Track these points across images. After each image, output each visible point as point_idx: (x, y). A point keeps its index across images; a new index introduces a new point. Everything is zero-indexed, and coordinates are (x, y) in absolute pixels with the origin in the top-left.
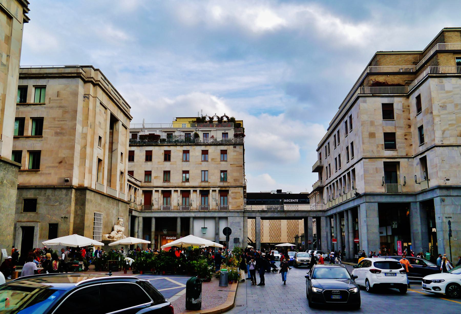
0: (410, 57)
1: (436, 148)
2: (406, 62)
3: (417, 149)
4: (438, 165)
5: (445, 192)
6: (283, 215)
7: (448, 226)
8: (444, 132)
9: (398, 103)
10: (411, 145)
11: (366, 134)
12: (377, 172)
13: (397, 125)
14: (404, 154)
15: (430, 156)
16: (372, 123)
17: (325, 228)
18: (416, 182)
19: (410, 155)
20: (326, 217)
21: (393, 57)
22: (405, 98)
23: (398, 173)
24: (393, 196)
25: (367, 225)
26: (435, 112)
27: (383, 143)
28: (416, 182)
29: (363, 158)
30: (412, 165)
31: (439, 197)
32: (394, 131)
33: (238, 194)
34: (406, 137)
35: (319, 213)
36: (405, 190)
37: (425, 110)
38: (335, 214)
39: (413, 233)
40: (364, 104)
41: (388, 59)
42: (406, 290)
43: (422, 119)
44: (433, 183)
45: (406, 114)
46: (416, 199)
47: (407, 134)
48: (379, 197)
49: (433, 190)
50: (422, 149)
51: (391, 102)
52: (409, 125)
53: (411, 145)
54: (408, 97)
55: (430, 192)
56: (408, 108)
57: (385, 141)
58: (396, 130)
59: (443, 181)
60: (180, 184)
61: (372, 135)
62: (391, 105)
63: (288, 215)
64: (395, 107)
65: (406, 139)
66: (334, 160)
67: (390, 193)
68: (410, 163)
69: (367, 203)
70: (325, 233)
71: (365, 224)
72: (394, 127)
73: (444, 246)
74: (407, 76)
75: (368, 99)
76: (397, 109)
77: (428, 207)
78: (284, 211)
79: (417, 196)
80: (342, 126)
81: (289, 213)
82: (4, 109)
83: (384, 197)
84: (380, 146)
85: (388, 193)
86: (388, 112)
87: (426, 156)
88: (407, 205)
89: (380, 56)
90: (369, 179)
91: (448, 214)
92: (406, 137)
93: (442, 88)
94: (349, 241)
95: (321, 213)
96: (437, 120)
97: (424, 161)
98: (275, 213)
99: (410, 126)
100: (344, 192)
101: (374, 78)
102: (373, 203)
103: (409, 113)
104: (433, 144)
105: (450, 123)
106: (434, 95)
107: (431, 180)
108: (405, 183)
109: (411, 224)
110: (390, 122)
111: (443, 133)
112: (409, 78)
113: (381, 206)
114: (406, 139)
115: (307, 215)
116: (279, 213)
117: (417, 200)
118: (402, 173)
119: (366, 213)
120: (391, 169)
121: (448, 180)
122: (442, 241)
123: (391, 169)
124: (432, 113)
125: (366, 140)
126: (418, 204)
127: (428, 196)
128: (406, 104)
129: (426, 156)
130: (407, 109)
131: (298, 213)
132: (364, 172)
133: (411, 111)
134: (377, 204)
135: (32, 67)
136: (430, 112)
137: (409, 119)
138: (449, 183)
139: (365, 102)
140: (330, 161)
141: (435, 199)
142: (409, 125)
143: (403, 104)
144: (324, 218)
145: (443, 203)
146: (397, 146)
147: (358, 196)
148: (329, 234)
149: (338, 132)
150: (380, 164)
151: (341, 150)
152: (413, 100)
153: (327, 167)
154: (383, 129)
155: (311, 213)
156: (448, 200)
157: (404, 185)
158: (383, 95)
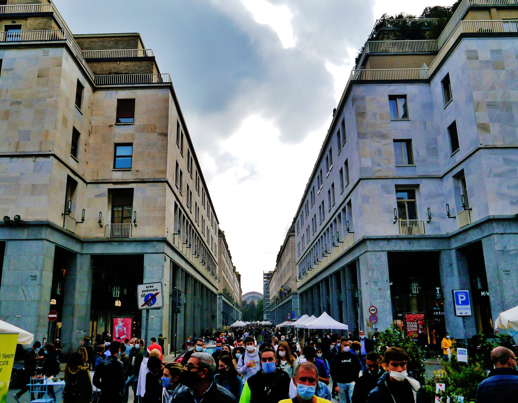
3: (444, 162)
18: (449, 215)
28: (449, 215)
33: (432, 211)
36: (429, 231)
42: (12, 221)
46: (82, 248)
49: (478, 226)
55: (134, 243)
60: (395, 173)
77: (473, 258)
82: (168, 115)
90: (376, 219)
94: (333, 301)
97: (460, 177)
100: (338, 240)
113: (392, 256)
127: (473, 237)
129: (463, 170)
135: (156, 180)
141: (146, 257)
149: (321, 172)
157: (428, 222)
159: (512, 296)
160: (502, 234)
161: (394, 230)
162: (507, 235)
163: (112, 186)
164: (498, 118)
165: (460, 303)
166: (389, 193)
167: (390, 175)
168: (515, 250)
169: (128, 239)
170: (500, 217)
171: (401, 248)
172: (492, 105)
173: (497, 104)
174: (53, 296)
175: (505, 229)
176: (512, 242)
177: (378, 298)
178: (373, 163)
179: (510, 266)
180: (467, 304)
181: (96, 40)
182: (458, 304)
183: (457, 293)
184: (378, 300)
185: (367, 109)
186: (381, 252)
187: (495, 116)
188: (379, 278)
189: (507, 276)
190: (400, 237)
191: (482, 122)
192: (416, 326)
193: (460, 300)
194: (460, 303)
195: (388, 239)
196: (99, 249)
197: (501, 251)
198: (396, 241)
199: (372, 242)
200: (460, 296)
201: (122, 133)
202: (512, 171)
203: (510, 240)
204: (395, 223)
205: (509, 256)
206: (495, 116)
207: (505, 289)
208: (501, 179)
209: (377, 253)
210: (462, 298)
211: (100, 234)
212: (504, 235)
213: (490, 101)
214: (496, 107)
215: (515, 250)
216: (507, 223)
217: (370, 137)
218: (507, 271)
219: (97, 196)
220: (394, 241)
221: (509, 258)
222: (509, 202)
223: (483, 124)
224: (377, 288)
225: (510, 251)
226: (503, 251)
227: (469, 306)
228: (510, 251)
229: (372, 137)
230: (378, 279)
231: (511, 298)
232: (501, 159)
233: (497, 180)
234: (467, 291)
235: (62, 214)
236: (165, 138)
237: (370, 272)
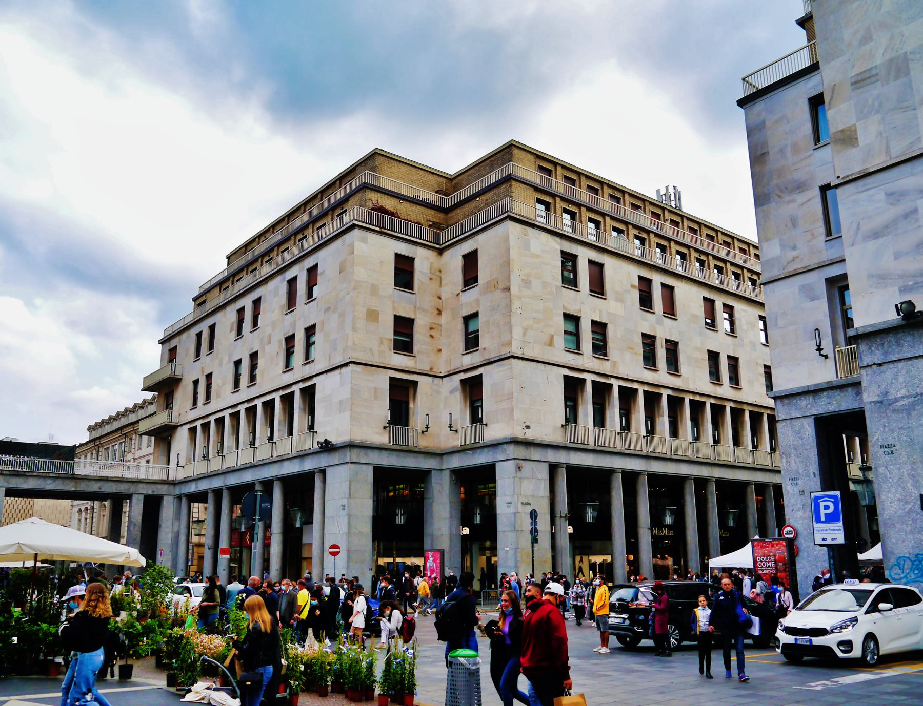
0: (432, 179)
1: (512, 360)
2: (424, 185)
4: (515, 394)
5: (521, 452)
6: (70, 487)
7: (529, 520)
8: (525, 330)
9: (423, 259)
10: (440, 351)
11: (361, 312)
12: (376, 398)
13: (418, 305)
14: (426, 368)
15: (491, 378)
16: (374, 290)
17: (169, 524)
18: (450, 427)
19: (436, 371)
20: (179, 498)
21: (405, 168)
22: (435, 253)
23: (411, 405)
24: (402, 454)
25: (349, 516)
26: (514, 290)
27: (392, 337)
29: (351, 362)
30: (439, 392)
31: (512, 461)
32: (411, 316)
34: (433, 333)
35: (159, 486)
36: (423, 443)
37: (488, 283)
38: (218, 493)
39: (432, 536)
40: (363, 245)
41: (397, 168)
43: (477, 301)
44: (494, 431)
45: (434, 285)
46: (442, 463)
47: (434, 326)
48: (376, 452)
50: (469, 360)
51: (411, 255)
52: (438, 309)
53: (440, 351)
54: (441, 252)
55: (486, 450)
56: (438, 273)
57: (396, 333)
58: (415, 314)
59: (520, 428)
61: (372, 315)
62: (410, 260)
63: (83, 487)
64: (417, 265)
65: (431, 336)
66: (232, 366)
67: (398, 447)
68: (434, 387)
69: (352, 465)
70: (170, 536)
71: (344, 513)
72: (412, 307)
73: (516, 562)
74: (432, 212)
75: (370, 235)
76: (421, 272)
78: (73, 478)
79: (445, 457)
80: (277, 289)
81: (86, 482)
83: (385, 453)
84: (386, 343)
85: (394, 447)
86: (404, 274)
87: (315, 385)
88: (423, 476)
89: (382, 158)
90: (350, 411)
91: (526, 496)
92: (433, 333)
93: (527, 246)
95: (166, 487)
96: (516, 305)
98: (49, 481)
99: (439, 312)
101: (374, 197)
102: (364, 466)
103: (440, 286)
104: (505, 352)
105: (535, 315)
106: (513, 255)
107: (490, 426)
108: (427, 428)
109: (427, 516)
110: (404, 295)
111: (524, 334)
112: (434, 217)
114: (431, 336)
115: (132, 491)
116: (59, 482)
117: (444, 467)
118: (419, 408)
119: (350, 489)
120: (401, 394)
121: (528, 427)
122: (511, 553)
123: (401, 394)
124: (508, 289)
125: (361, 323)
126: (448, 472)
128: (436, 266)
129: (315, 385)
130: (437, 275)
131: (110, 484)
132: (352, 394)
133: (443, 283)
134: (371, 469)
136: (501, 286)
137: (440, 298)
138: (530, 435)
139: (364, 240)
140: (190, 370)
141: (498, 466)
142: (438, 309)
143: (431, 263)
144: (171, 498)
145: (519, 474)
146: (416, 348)
147: (327, 447)
148: (183, 538)
149: (257, 303)
150: (382, 381)
151: (267, 338)
152: (454, 259)
153: (196, 383)
154: (394, 308)
155: (141, 485)
156: (526, 466)
158: (400, 235)
159: (899, 500)
160: (880, 365)
161: (383, 439)
162: (891, 366)
163: (463, 376)
164: (876, 104)
165: (823, 518)
166: (812, 299)
167: (813, 262)
168: (908, 397)
169: (478, 445)
170: (871, 330)
171: (840, 405)
172: (863, 80)
173: (874, 72)
174: (466, 520)
175: (886, 354)
176: (901, 379)
177: (799, 510)
178: (783, 247)
179: (895, 434)
180: (837, 520)
181: (472, 171)
182: (818, 520)
183: (817, 498)
184: (800, 514)
185: (770, 144)
186: (801, 420)
187: (870, 102)
188: (801, 471)
189: (887, 457)
190: (834, 384)
191: (841, 128)
192: (772, 564)
193: (823, 512)
194: (823, 518)
195: (814, 392)
196: (456, 462)
197: (876, 402)
198: (831, 393)
199: (786, 401)
200: (822, 505)
201: (470, 300)
202: (906, 216)
203: (896, 376)
204: (385, 428)
205: (894, 411)
206: (870, 102)
207: (884, 486)
208: (881, 241)
209: (795, 422)
210: (827, 507)
211: (455, 442)
212: (884, 368)
213: (859, 71)
214: (873, 79)
215: (908, 397)
216: (891, 338)
217: (777, 198)
218: (889, 446)
219: (451, 392)
220: (825, 393)
221: (894, 416)
222: (897, 288)
223: (842, 131)
224: (796, 490)
225: (896, 400)
226: (881, 402)
227: (840, 525)
228: (896, 400)
229: (779, 196)
230: (798, 472)
231: (895, 505)
232: (881, 196)
233: (872, 245)
234: (838, 493)
235: (385, 428)
236: (508, 294)
237: (784, 460)
